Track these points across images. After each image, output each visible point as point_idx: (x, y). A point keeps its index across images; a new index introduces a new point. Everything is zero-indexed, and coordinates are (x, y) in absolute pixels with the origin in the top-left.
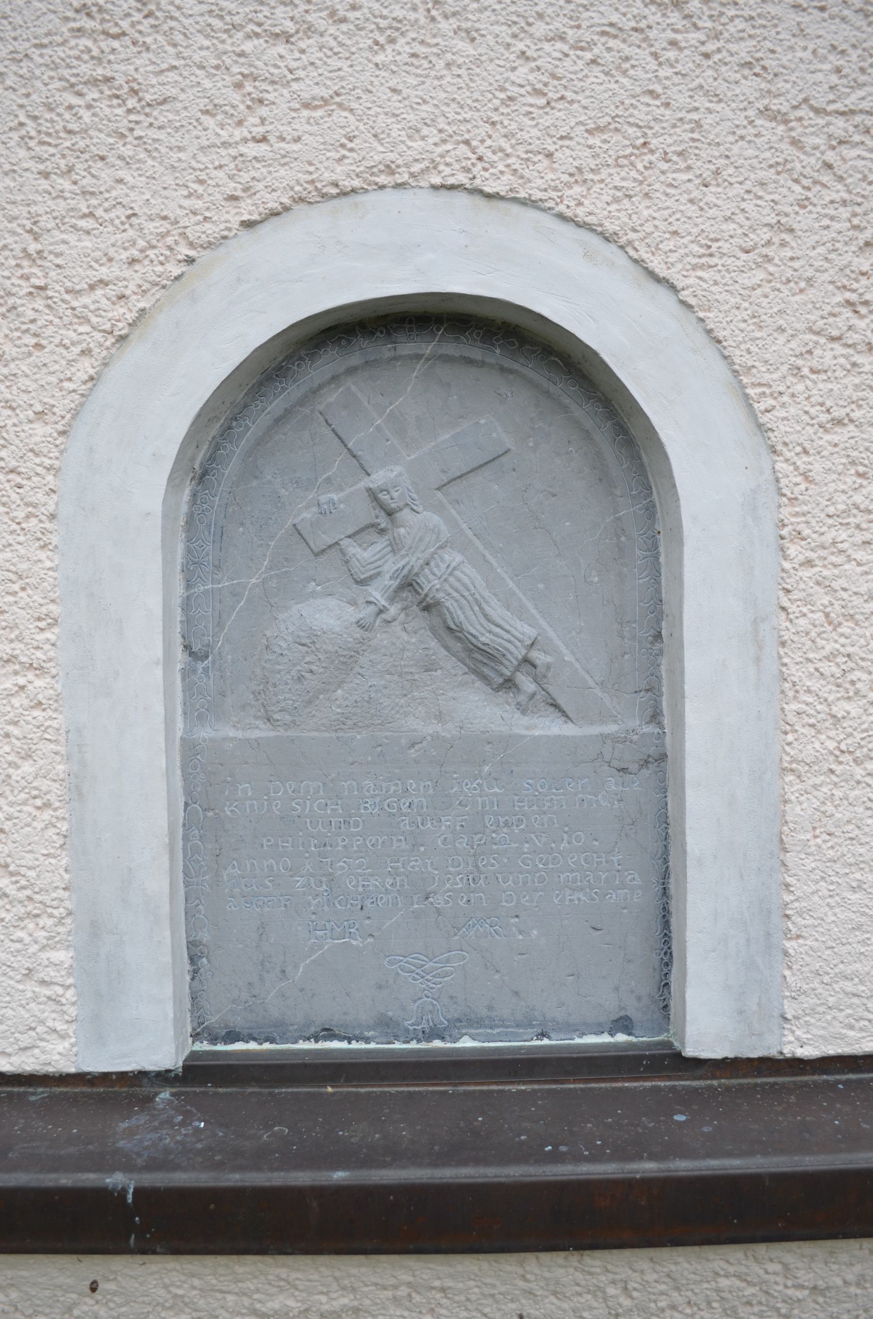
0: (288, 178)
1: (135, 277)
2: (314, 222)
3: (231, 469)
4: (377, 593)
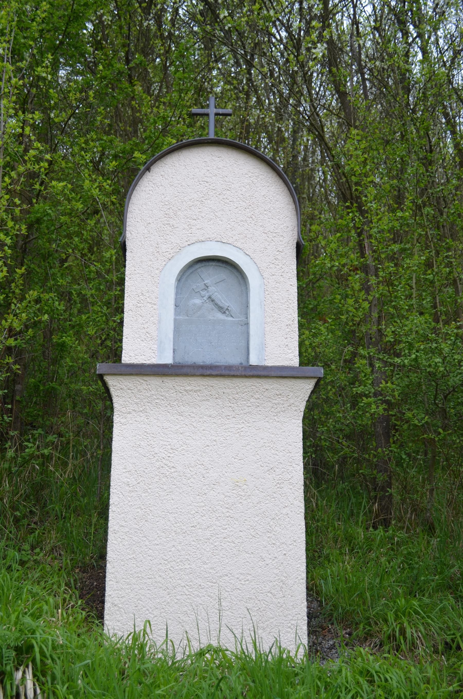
0: (195, 239)
1: (172, 251)
2: (199, 245)
3: (183, 280)
4: (205, 298)
